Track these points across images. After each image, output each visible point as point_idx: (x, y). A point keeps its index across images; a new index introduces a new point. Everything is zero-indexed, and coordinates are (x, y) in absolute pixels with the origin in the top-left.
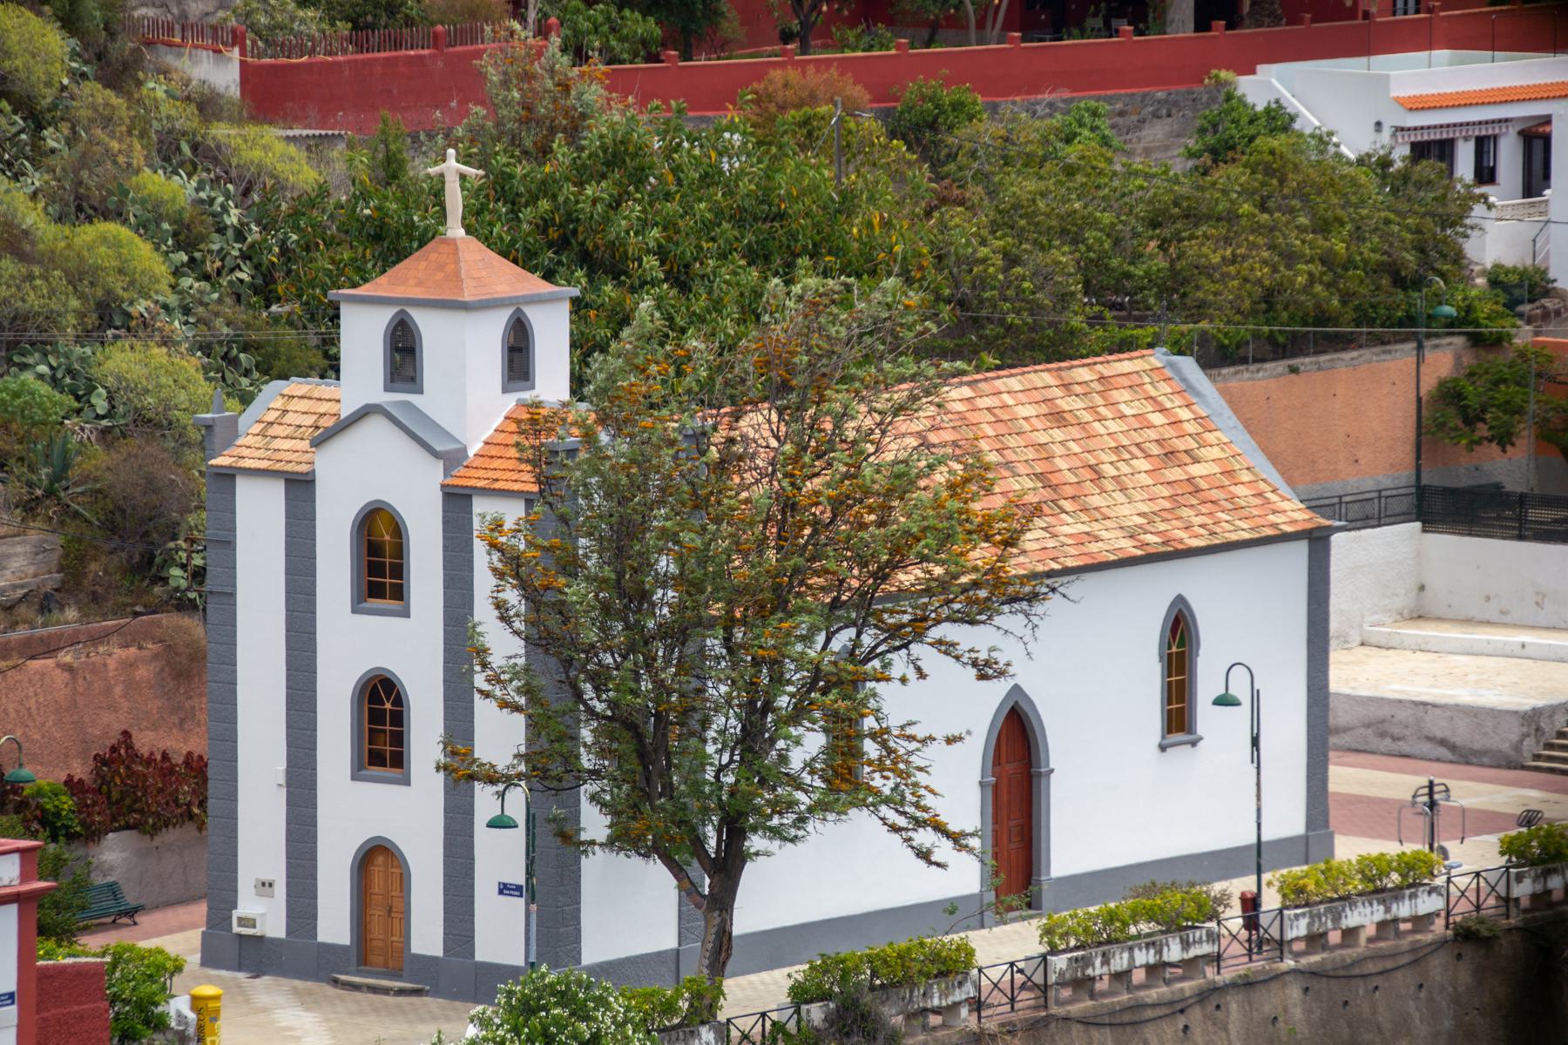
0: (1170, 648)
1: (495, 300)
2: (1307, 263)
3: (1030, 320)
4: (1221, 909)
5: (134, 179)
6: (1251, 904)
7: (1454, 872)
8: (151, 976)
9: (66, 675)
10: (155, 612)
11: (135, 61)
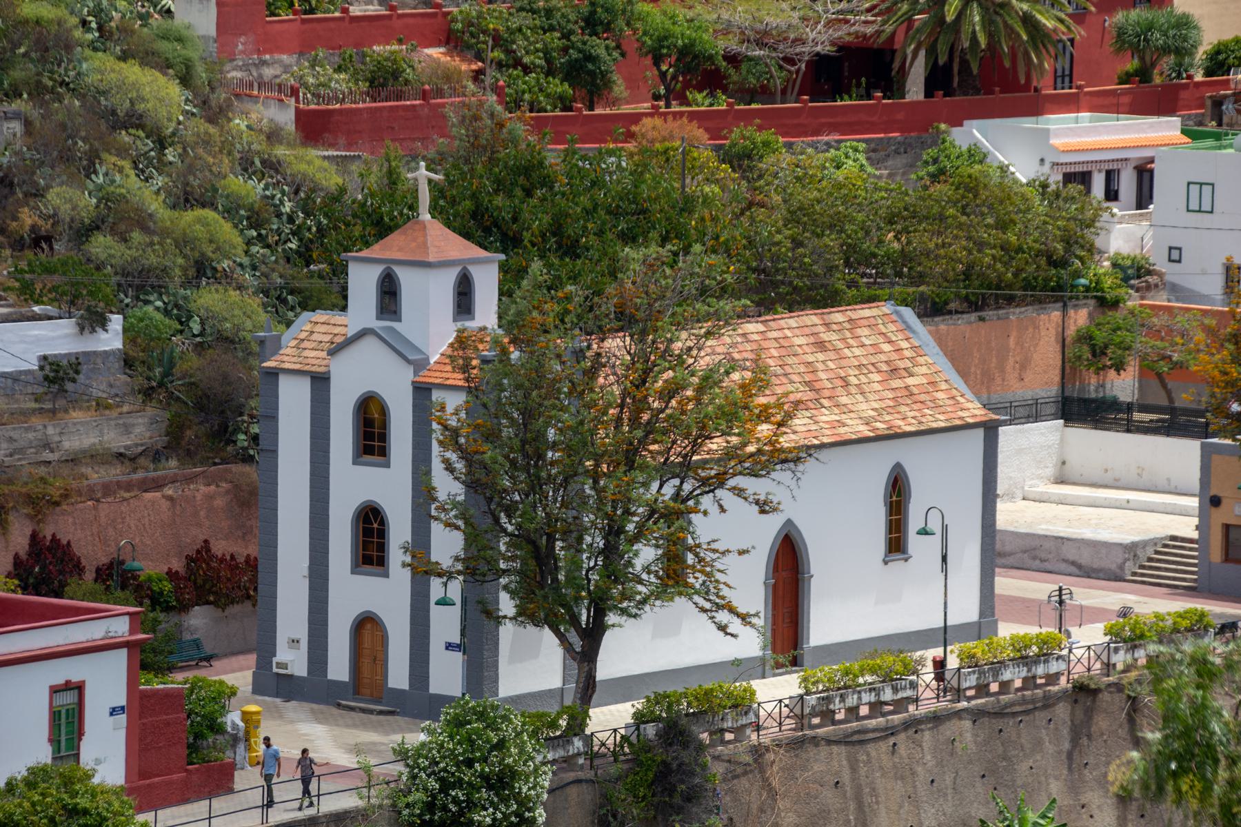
0: (891, 497)
1: (450, 261)
2: (991, 249)
3: (808, 283)
4: (920, 668)
5: (223, 182)
6: (940, 665)
7: (1074, 646)
8: (214, 698)
9: (168, 502)
10: (227, 463)
11: (228, 106)
